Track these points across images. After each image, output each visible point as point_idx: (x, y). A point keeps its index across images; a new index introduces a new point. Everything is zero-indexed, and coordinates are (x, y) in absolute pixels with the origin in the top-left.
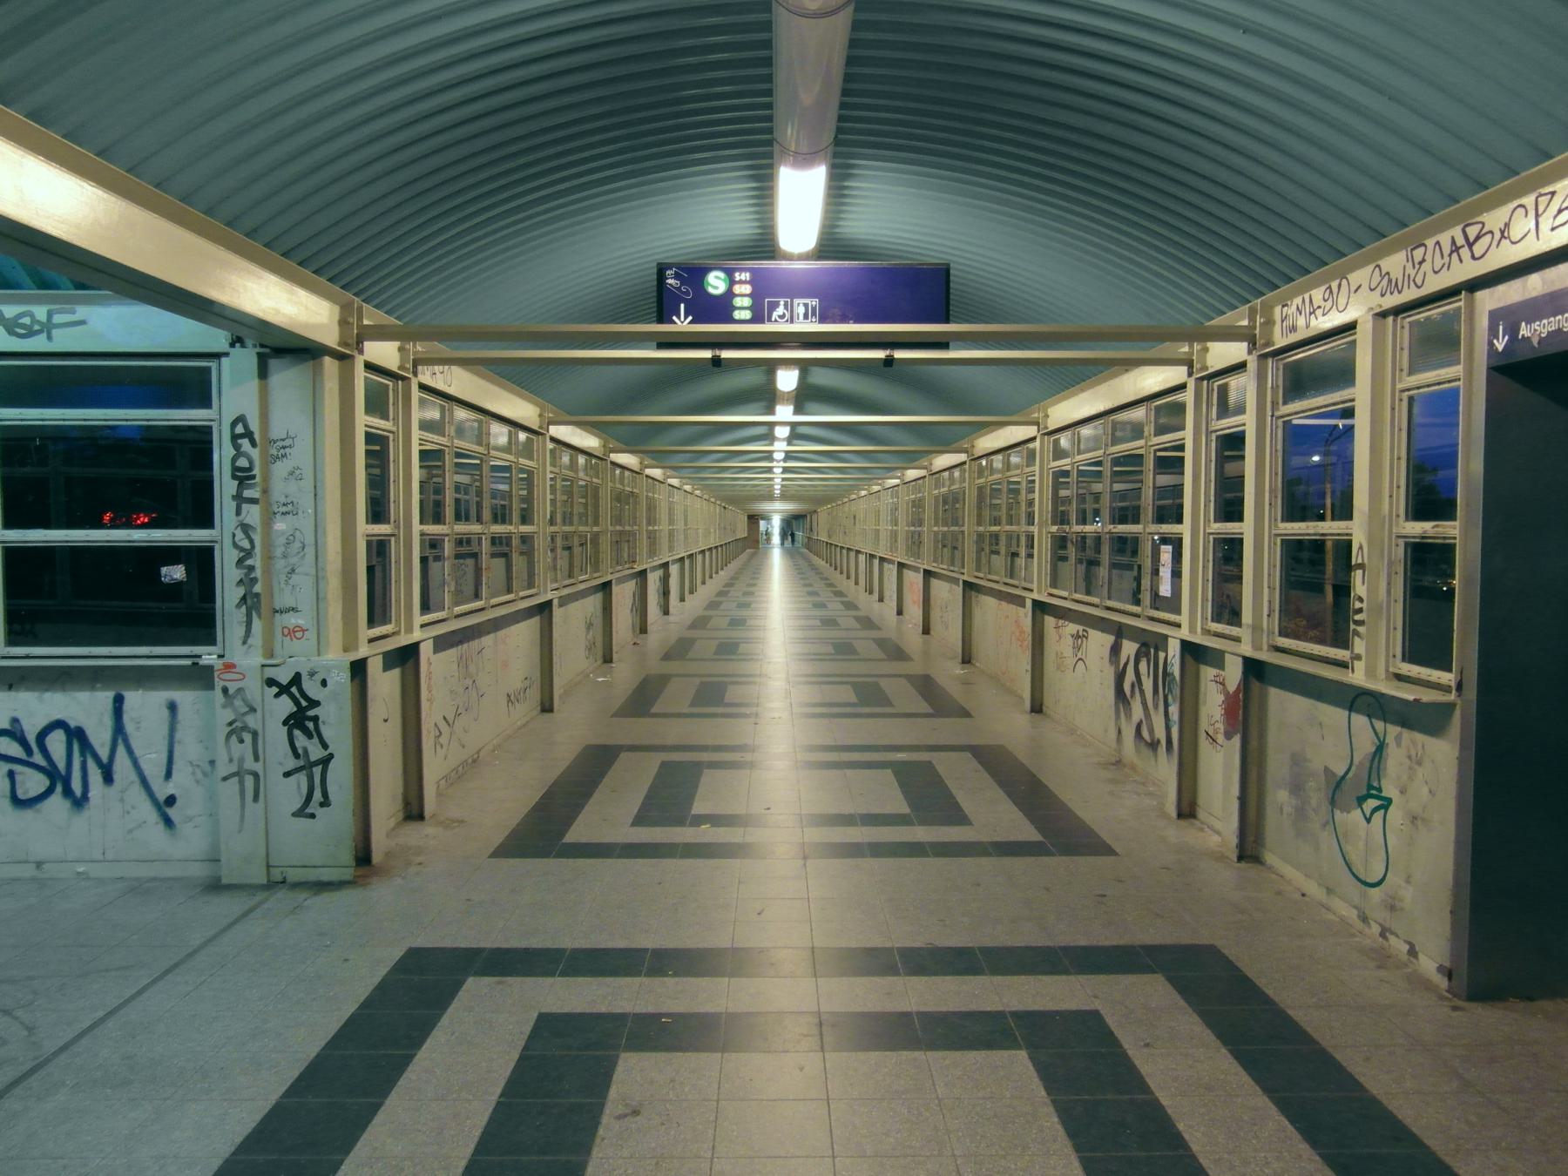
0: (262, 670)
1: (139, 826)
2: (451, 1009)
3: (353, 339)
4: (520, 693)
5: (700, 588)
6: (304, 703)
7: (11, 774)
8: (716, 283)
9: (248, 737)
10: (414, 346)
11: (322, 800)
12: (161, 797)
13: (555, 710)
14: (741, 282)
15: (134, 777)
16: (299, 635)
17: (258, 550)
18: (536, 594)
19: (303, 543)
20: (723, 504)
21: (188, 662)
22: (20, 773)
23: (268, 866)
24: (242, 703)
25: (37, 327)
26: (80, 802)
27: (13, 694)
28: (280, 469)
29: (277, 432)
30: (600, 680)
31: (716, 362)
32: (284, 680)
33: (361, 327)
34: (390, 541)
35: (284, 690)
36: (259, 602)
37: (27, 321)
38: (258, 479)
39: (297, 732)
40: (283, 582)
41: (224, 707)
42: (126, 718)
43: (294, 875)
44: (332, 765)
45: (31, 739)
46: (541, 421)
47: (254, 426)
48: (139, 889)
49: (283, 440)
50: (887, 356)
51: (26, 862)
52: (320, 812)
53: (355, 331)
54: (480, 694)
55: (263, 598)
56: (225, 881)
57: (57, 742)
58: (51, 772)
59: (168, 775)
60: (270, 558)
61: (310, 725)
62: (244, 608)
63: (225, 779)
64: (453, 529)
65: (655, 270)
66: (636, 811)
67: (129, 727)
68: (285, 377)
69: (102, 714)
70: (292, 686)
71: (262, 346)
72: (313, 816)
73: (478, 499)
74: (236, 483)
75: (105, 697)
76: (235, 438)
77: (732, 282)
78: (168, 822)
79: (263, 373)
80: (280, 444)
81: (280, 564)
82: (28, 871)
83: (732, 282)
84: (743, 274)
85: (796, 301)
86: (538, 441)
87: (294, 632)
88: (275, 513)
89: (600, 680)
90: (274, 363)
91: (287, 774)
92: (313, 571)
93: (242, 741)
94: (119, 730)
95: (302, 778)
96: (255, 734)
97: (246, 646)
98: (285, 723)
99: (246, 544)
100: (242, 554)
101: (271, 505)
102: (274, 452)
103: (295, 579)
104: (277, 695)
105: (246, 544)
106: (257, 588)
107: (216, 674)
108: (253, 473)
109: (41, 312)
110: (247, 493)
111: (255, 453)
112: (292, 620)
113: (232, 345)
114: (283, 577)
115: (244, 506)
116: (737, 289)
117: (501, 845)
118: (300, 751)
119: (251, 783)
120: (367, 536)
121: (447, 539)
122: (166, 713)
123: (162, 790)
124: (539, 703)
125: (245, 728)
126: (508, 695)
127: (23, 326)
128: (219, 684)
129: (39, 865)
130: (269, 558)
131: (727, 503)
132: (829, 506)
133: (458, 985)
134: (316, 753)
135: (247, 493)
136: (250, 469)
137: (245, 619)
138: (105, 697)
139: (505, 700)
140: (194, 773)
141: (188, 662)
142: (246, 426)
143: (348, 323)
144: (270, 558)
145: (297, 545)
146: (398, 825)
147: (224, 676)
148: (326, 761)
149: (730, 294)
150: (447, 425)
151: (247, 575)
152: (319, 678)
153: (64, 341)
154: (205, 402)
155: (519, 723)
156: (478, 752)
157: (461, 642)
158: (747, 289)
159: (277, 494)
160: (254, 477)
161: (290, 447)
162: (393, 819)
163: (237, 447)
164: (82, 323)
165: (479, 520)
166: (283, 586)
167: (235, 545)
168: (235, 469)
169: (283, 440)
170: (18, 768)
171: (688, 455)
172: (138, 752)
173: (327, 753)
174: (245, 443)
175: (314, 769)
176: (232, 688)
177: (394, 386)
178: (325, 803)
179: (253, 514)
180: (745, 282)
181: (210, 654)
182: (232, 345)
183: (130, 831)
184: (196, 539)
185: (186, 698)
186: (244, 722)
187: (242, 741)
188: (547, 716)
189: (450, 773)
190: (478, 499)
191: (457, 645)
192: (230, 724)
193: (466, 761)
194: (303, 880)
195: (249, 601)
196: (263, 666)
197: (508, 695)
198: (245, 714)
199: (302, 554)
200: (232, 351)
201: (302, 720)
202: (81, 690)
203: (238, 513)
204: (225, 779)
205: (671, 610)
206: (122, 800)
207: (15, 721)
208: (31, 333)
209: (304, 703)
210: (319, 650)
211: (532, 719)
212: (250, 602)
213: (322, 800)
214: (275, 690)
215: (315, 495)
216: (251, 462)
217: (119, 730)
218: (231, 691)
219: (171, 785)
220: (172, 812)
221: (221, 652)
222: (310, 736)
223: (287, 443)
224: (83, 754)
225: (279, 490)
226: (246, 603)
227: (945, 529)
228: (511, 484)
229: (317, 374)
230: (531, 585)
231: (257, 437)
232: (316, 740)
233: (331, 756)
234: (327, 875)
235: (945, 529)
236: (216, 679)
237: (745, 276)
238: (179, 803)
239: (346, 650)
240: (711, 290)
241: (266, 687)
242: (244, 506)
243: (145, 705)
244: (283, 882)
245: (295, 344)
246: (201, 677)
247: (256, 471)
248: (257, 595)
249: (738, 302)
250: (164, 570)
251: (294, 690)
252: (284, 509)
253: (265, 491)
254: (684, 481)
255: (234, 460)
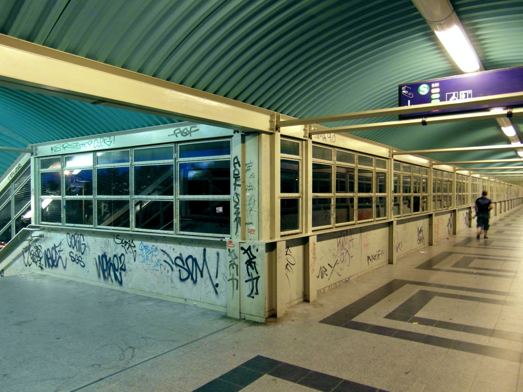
0: (240, 244)
1: (209, 292)
2: (246, 387)
3: (274, 127)
4: (375, 256)
5: (513, 208)
6: (251, 257)
7: (180, 271)
8: (423, 90)
9: (235, 267)
10: (310, 127)
11: (256, 292)
12: (215, 284)
13: (393, 263)
14: (435, 88)
15: (208, 276)
16: (253, 232)
17: (240, 202)
18: (387, 219)
19: (254, 200)
20: (510, 184)
21: (219, 240)
22: (182, 271)
23: (240, 313)
24: (234, 255)
25: (188, 133)
26: (195, 282)
27: (180, 246)
28: (248, 174)
29: (247, 162)
30: (422, 252)
31: (424, 123)
32: (246, 248)
33: (393, 152)
34: (299, 199)
35: (246, 252)
36: (240, 220)
37: (185, 131)
38: (240, 178)
39: (249, 267)
40: (248, 213)
41: (229, 256)
42: (206, 257)
43: (248, 318)
44: (259, 279)
45: (184, 260)
46: (389, 154)
47: (240, 160)
48: (205, 313)
49: (249, 164)
50: (508, 112)
51: (183, 298)
52: (255, 296)
53: (275, 124)
54: (351, 256)
55: (242, 219)
56: (228, 315)
57: (190, 261)
58: (188, 271)
59: (217, 277)
60: (245, 205)
61: (253, 265)
62: (236, 222)
63: (229, 280)
64: (335, 195)
65: (398, 88)
66: (391, 311)
67: (207, 260)
68: (250, 142)
69: (201, 254)
70: (247, 251)
71: (242, 132)
72: (253, 297)
73: (419, 186)
74: (235, 179)
75: (201, 249)
76: (235, 164)
77: (431, 88)
78: (216, 292)
79: (243, 141)
80: (248, 165)
81: (248, 207)
82: (183, 301)
83: (431, 88)
84: (436, 84)
85: (461, 92)
86: (388, 162)
87: (251, 231)
88: (246, 190)
89: (422, 252)
90: (247, 137)
91: (246, 281)
92: (257, 210)
93: (233, 268)
94: (205, 260)
95: (250, 283)
96: (237, 266)
97: (237, 235)
98: (246, 263)
99: (237, 200)
100: (236, 204)
101: (245, 187)
102: (246, 168)
103: (252, 213)
104: (244, 253)
105: (237, 200)
106: (240, 216)
107: (227, 244)
108: (239, 176)
109: (188, 128)
110: (238, 183)
111: (240, 169)
112: (251, 227)
113: (234, 132)
114: (248, 212)
115: (237, 187)
116: (433, 91)
117: (328, 318)
118: (250, 274)
119: (235, 282)
120: (281, 197)
121: (332, 198)
122: (216, 256)
123: (215, 282)
124: (388, 260)
125: (234, 264)
126: (368, 257)
127: (185, 133)
128: (228, 248)
129: (186, 300)
130: (244, 205)
131: (511, 184)
132: (517, 186)
133: (261, 375)
134: (255, 275)
135: (238, 183)
136: (238, 174)
137: (236, 226)
138: (201, 249)
139: (367, 258)
140: (223, 277)
141: (219, 240)
142: (238, 160)
143: (272, 121)
144: (245, 205)
145: (253, 201)
146: (299, 303)
147: (229, 245)
148: (257, 278)
149: (430, 93)
150: (333, 157)
151: (237, 211)
152: (256, 248)
153: (195, 136)
154: (228, 153)
155: (375, 268)
156: (349, 278)
157: (340, 237)
158: (438, 90)
159: (247, 184)
160: (239, 177)
161: (251, 166)
162: (297, 301)
163: (235, 167)
164: (198, 130)
165: (441, 192)
166: (248, 215)
167: (234, 200)
168: (235, 175)
169: (249, 164)
170: (181, 269)
171: (485, 170)
172: (209, 268)
173: (258, 275)
174: (237, 165)
175: (254, 281)
176: (231, 249)
177: (301, 143)
178: (257, 293)
179: (239, 190)
180: (437, 87)
181: (228, 237)
182: (234, 132)
183: (207, 293)
184: (221, 198)
185: (221, 251)
186: (234, 262)
187: (233, 268)
188: (391, 265)
189: (331, 285)
190: (419, 186)
191: (337, 238)
192: (230, 262)
193: (342, 281)
194: (250, 320)
195: (237, 220)
196: (240, 243)
197: (368, 257)
198: (234, 259)
199: (254, 204)
200: (234, 134)
201: (250, 263)
202: (195, 246)
203: (235, 190)
204: (229, 280)
205: (472, 225)
206: (205, 283)
207: (181, 254)
208: (187, 135)
209: (251, 257)
210: (259, 238)
211: (383, 266)
212: (238, 220)
213: (256, 292)
214: (243, 251)
215: (258, 183)
216: (239, 172)
217: (205, 260)
218: (231, 251)
219: (217, 280)
220: (217, 289)
221: (230, 237)
222: (253, 269)
223: (250, 165)
224: (196, 267)
225: (248, 181)
226: (236, 221)
227: (464, 194)
228: (411, 179)
229: (259, 141)
230: (385, 216)
231: (240, 163)
232: (254, 270)
233: (259, 277)
234: (257, 319)
235: (464, 194)
236: (227, 246)
237: (437, 85)
238: (219, 286)
239: (271, 239)
240: (422, 93)
241: (241, 250)
242: (237, 187)
243: (211, 252)
244: (244, 319)
245: (253, 131)
246: (222, 244)
247: (240, 175)
248: (240, 218)
249: (433, 96)
250: (217, 208)
251: (249, 252)
252: (249, 188)
253: (244, 182)
254: (482, 175)
255: (234, 171)
